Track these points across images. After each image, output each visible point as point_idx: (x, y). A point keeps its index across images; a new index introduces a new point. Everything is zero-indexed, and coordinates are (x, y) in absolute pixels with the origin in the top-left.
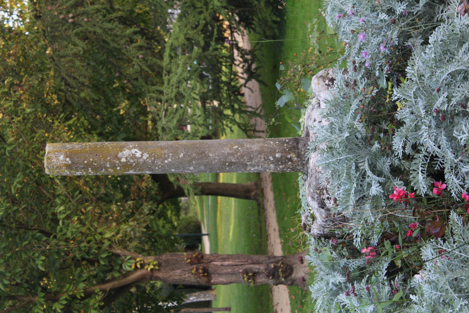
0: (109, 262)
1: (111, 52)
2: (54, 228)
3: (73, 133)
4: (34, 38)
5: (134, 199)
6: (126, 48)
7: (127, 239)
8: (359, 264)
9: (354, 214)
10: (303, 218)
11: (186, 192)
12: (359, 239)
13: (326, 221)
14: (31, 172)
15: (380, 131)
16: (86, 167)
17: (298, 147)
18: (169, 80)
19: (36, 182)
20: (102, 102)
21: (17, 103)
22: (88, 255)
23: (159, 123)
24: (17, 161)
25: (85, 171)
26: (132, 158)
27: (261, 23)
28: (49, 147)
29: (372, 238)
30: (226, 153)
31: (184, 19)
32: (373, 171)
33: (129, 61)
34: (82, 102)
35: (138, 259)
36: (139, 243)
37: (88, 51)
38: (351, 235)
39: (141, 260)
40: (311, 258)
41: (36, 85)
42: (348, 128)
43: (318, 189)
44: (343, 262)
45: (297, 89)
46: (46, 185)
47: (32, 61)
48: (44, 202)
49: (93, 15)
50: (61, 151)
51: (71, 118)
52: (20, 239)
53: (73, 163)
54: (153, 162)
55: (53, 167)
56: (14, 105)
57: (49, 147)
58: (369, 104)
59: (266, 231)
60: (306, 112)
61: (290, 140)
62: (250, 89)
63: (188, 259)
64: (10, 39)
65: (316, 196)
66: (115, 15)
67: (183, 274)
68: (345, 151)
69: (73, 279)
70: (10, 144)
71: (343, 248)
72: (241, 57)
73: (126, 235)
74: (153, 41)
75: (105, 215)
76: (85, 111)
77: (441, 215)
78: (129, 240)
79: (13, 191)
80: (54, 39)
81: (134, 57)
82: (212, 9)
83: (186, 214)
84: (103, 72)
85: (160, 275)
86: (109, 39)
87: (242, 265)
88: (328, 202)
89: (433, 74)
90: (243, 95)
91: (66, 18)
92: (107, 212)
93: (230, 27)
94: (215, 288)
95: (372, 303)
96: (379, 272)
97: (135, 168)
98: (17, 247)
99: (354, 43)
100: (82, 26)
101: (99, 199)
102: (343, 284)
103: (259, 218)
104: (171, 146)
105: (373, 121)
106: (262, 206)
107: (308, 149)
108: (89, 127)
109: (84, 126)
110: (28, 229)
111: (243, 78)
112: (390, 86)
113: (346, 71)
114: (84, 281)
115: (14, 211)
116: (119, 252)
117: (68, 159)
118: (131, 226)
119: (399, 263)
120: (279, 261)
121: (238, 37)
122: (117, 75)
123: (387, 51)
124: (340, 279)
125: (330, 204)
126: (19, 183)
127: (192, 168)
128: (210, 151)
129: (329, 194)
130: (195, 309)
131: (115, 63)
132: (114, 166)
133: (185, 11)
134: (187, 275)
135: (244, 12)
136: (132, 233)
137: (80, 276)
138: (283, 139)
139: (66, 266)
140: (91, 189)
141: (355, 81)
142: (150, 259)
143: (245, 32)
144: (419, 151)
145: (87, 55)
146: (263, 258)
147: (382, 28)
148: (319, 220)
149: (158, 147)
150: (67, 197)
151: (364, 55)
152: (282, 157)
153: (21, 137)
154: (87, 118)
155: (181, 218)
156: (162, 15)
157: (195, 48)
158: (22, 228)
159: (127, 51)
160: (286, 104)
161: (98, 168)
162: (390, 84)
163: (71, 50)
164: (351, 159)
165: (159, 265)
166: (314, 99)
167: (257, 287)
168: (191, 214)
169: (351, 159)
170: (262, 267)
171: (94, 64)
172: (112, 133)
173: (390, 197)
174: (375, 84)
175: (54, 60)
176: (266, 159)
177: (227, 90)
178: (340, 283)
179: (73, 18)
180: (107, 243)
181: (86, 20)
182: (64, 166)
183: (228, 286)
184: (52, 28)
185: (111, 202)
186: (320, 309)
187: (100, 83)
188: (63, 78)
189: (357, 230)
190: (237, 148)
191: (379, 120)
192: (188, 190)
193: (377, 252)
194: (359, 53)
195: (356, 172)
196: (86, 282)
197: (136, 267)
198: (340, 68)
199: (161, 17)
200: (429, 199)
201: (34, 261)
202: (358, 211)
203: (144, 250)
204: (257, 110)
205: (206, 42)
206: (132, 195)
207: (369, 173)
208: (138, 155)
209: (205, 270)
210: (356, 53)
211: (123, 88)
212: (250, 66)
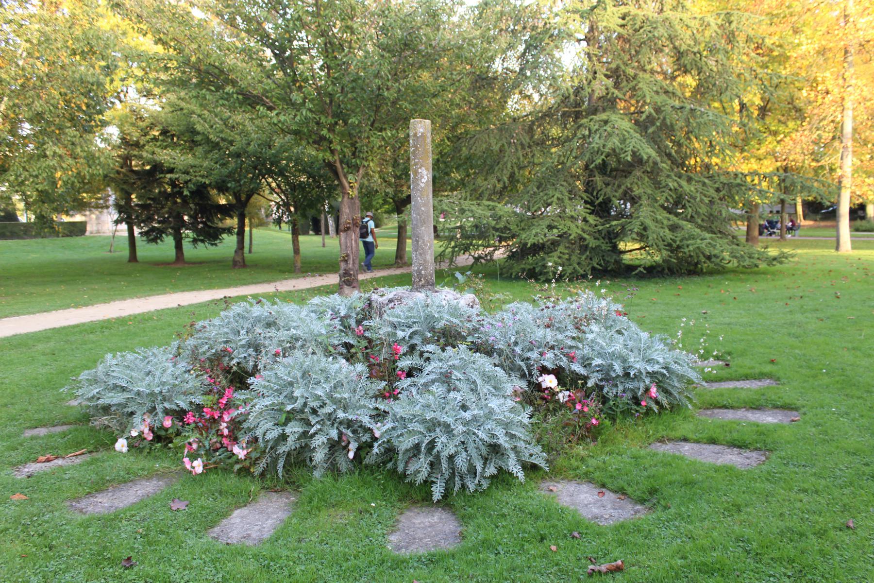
1: (492, 167)
2: (376, 129)
15: (438, 337)
16: (415, 146)
32: (412, 333)
33: (485, 180)
40: (356, 294)
44: (354, 315)
57: (428, 122)
77: (384, 376)
80: (500, 130)
84: (479, 163)
85: (346, 199)
86: (500, 166)
89: (475, 370)
93: (508, 245)
97: (415, 178)
113: (478, 315)
119: (353, 350)
121: (502, 250)
124: (343, 313)
132: (415, 164)
137: (345, 146)
139: (351, 137)
142: (356, 192)
143: (505, 256)
144: (425, 361)
146: (357, 266)
148: (381, 300)
163: (493, 141)
165: (352, 198)
167: (338, 264)
168: (385, 221)
170: (351, 266)
172: (439, 168)
174: (469, 334)
176: (420, 265)
180: (366, 164)
185: (393, 167)
189: (374, 322)
200: (394, 369)
207: (411, 330)
208: (423, 180)
209: (348, 228)
211: (468, 176)
212: (483, 258)
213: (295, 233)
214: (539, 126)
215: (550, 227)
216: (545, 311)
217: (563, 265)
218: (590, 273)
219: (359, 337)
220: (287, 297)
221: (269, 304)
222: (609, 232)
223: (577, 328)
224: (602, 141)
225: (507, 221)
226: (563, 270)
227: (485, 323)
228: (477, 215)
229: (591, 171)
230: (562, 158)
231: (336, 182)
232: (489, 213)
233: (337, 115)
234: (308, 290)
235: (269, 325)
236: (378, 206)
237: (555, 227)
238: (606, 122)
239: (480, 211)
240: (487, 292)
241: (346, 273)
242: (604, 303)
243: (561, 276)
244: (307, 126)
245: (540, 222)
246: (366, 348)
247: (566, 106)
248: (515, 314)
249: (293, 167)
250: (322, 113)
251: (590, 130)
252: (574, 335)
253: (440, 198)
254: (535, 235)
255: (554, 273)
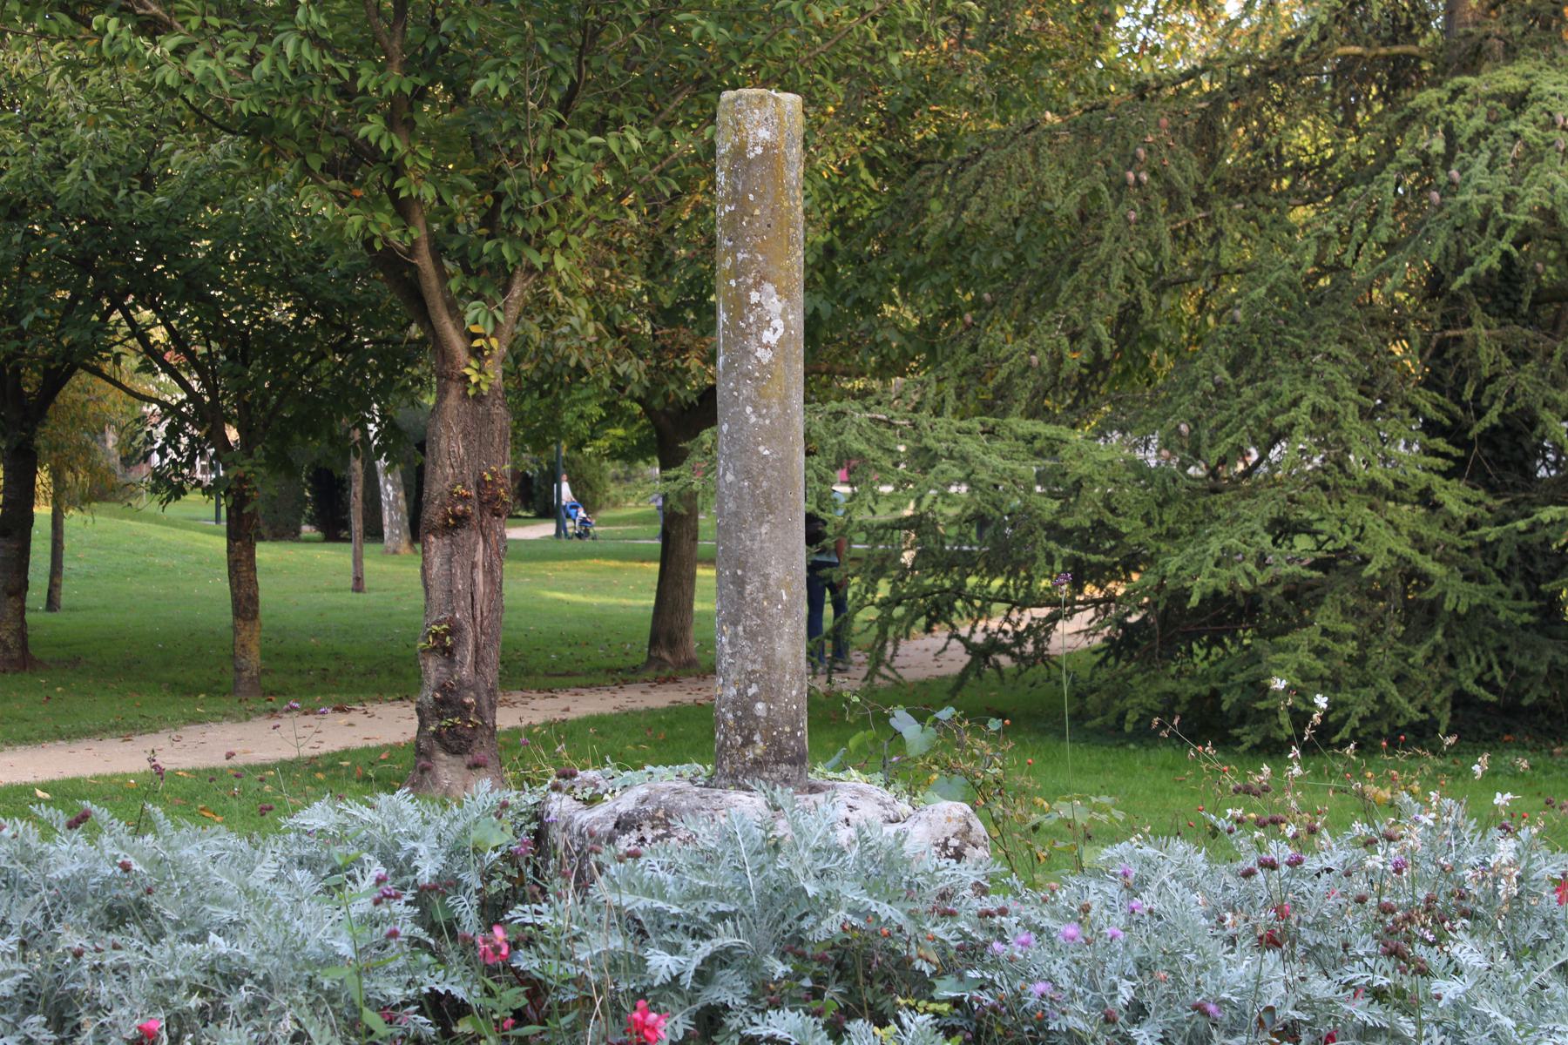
0: (489, 266)
1: (1047, 281)
2: (582, 121)
3: (836, 180)
4: (1087, 82)
5: (655, 337)
6: (1057, 322)
7: (550, 316)
8: (465, 921)
9: (597, 908)
10: (591, 774)
11: (672, 473)
12: (528, 919)
13: (581, 834)
14: (732, 63)
15: (819, 979)
16: (737, 197)
17: (784, 763)
18: (969, 432)
19: (707, 77)
20: (920, 260)
21: (915, 31)
22: (507, 211)
23: (857, 405)
24: (763, 29)
25: (727, 195)
26: (759, 318)
27: (1120, 679)
28: (792, 103)
29: (534, 955)
30: (770, 570)
31: (1132, 475)
33: (1020, 331)
34: (915, 202)
35: (494, 342)
36: (538, 348)
37: (1051, 223)
38: (541, 899)
39: (491, 349)
40: (483, 790)
41: (961, 84)
42: (829, 893)
43: (668, 815)
44: (472, 879)
45: (936, 763)
46: (697, 103)
47: (1027, 77)
48: (652, 97)
49: (1145, 235)
50: (781, 133)
51: (874, 174)
52: (555, 33)
53: (750, 162)
54: (748, 375)
55: (739, 112)
56: (909, 24)
57: (791, 101)
58: (893, 951)
59: (565, 688)
60: (874, 787)
61: (800, 741)
62: (945, 649)
63: (493, 474)
64: (1085, 19)
65: (650, 809)
66: (1145, 293)
67: (454, 461)
68: (768, 885)
69: (445, 172)
70: (806, 13)
71: (509, 879)
72: (1029, 626)
73: (560, 313)
74: (1075, 393)
75: (614, 258)
76: (892, 211)
78: (546, 320)
79: (681, 17)
80: (1084, 132)
81: (1032, 342)
82: (1158, 550)
83: (616, 478)
84: (996, 263)
85: (452, 400)
86: (1081, 276)
87: (474, 619)
88: (633, 841)
90: (928, 629)
91: (1137, 165)
92: (622, 264)
93: (1110, 599)
94: (416, 552)
95: (359, 952)
96: (441, 974)
97: (733, 326)
98: (533, 24)
99: (1054, 914)
100: (1116, 206)
101: (658, 243)
102: (411, 878)
103: (599, 669)
104: (788, 424)
105: (847, 960)
106: (632, 677)
107: (774, 789)
108: (850, 223)
109: (854, 207)
110: (581, 55)
111: (973, 631)
112: (938, 1007)
114: (440, 199)
115: (628, 18)
116: (516, 291)
117: (759, 150)
118: (583, 327)
119: (464, 1027)
120: (482, 719)
121: (1083, 618)
122: (986, 296)
123: (1031, 1002)
124: (427, 870)
125: (626, 842)
126: (704, 32)
127: (730, 477)
128: (774, 526)
129: (654, 841)
130: (360, 495)
131: (1018, 290)
132: (738, 271)
133: (1153, 479)
134: (449, 471)
135: (1150, 637)
136: (565, 330)
137: (454, 188)
138: (804, 724)
139: (481, 153)
140: (686, 223)
141: (952, 914)
142: (494, 373)
143: (1097, 641)
145: (1041, 219)
146: (491, 674)
147: (1095, 989)
148: (584, 817)
149: (788, 389)
150: (664, 157)
151: (1023, 938)
152: (756, 718)
153: (825, 40)
154: (875, 215)
155: (606, 463)
156: (1143, 418)
157: (1056, 504)
158: (584, 36)
159: (1049, 323)
160: (898, 734)
161: (735, 230)
162: (946, 1007)
163: (1053, 177)
164: (745, 901)
165: (479, 398)
166: (910, 809)
167: (413, 662)
168: (613, 490)
169: (745, 901)
170: (466, 672)
171: (1018, 239)
172: (832, 280)
173: (642, 1004)
174: (946, 968)
175: (1028, 131)
177: (942, 586)
178: (416, 869)
179: (1138, 183)
180: (539, 261)
181: (1133, 216)
182: (741, 140)
183: (421, 587)
184: (1113, 127)
185: (650, 275)
186: (348, 816)
187: (966, 253)
188: (980, 155)
189: (553, 914)
190: (780, 600)
191: (848, 977)
192: (677, 478)
193: (499, 970)
194: (1029, 926)
195: (709, 913)
196: (436, 205)
197: (475, 336)
198: (993, 879)
199: (1139, 416)
201: (496, 69)
202: (605, 917)
203: (518, 359)
204: (888, 666)
205: (1070, 532)
206: (666, 331)
207: (706, 948)
208: (768, 336)
209: (461, 520)
210: (1028, 918)
211: (952, 313)
212: (1004, 649)
213: (243, 532)
214: (1242, 117)
215: (1283, 529)
216: (1260, 876)
217: (1331, 684)
218: (1445, 718)
219: (491, 971)
220: (201, 796)
221: (120, 827)
222: (1525, 552)
223: (1394, 953)
224: (1500, 182)
225: (1107, 499)
226: (1333, 706)
227: (1009, 922)
228: (984, 475)
229: (1456, 299)
230: (1335, 249)
231: (415, 331)
232: (1031, 468)
233: (422, 62)
234: (286, 767)
235: (117, 917)
236: (583, 428)
237: (1306, 528)
238: (1518, 102)
239: (995, 460)
240: (1022, 792)
241: (448, 701)
242: (1505, 850)
243: (1325, 731)
244: (302, 103)
245: (1242, 507)
246: (520, 1017)
247: (1353, 37)
248: (1133, 888)
249: (241, 263)
250: (365, 49)
251: (1450, 135)
252: (1381, 981)
253: (833, 405)
254: (1222, 556)
255: (1300, 718)
